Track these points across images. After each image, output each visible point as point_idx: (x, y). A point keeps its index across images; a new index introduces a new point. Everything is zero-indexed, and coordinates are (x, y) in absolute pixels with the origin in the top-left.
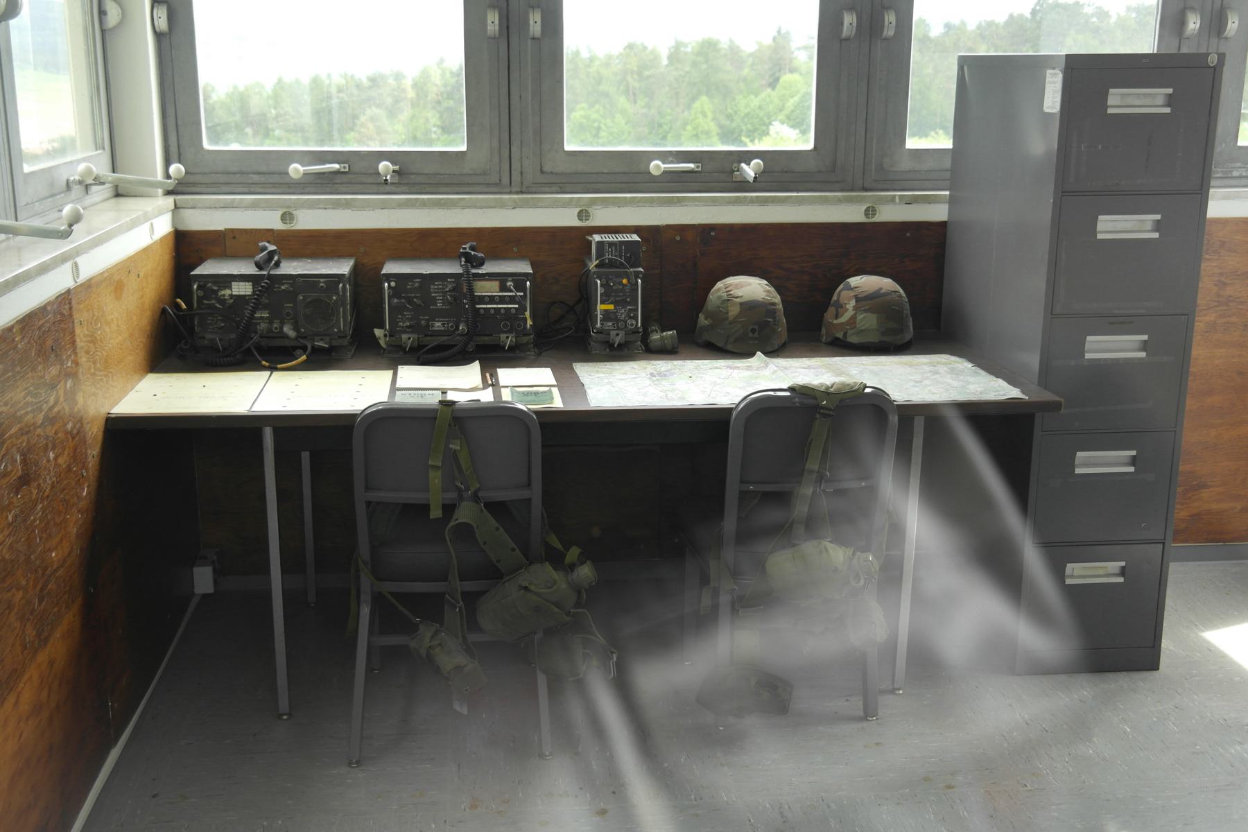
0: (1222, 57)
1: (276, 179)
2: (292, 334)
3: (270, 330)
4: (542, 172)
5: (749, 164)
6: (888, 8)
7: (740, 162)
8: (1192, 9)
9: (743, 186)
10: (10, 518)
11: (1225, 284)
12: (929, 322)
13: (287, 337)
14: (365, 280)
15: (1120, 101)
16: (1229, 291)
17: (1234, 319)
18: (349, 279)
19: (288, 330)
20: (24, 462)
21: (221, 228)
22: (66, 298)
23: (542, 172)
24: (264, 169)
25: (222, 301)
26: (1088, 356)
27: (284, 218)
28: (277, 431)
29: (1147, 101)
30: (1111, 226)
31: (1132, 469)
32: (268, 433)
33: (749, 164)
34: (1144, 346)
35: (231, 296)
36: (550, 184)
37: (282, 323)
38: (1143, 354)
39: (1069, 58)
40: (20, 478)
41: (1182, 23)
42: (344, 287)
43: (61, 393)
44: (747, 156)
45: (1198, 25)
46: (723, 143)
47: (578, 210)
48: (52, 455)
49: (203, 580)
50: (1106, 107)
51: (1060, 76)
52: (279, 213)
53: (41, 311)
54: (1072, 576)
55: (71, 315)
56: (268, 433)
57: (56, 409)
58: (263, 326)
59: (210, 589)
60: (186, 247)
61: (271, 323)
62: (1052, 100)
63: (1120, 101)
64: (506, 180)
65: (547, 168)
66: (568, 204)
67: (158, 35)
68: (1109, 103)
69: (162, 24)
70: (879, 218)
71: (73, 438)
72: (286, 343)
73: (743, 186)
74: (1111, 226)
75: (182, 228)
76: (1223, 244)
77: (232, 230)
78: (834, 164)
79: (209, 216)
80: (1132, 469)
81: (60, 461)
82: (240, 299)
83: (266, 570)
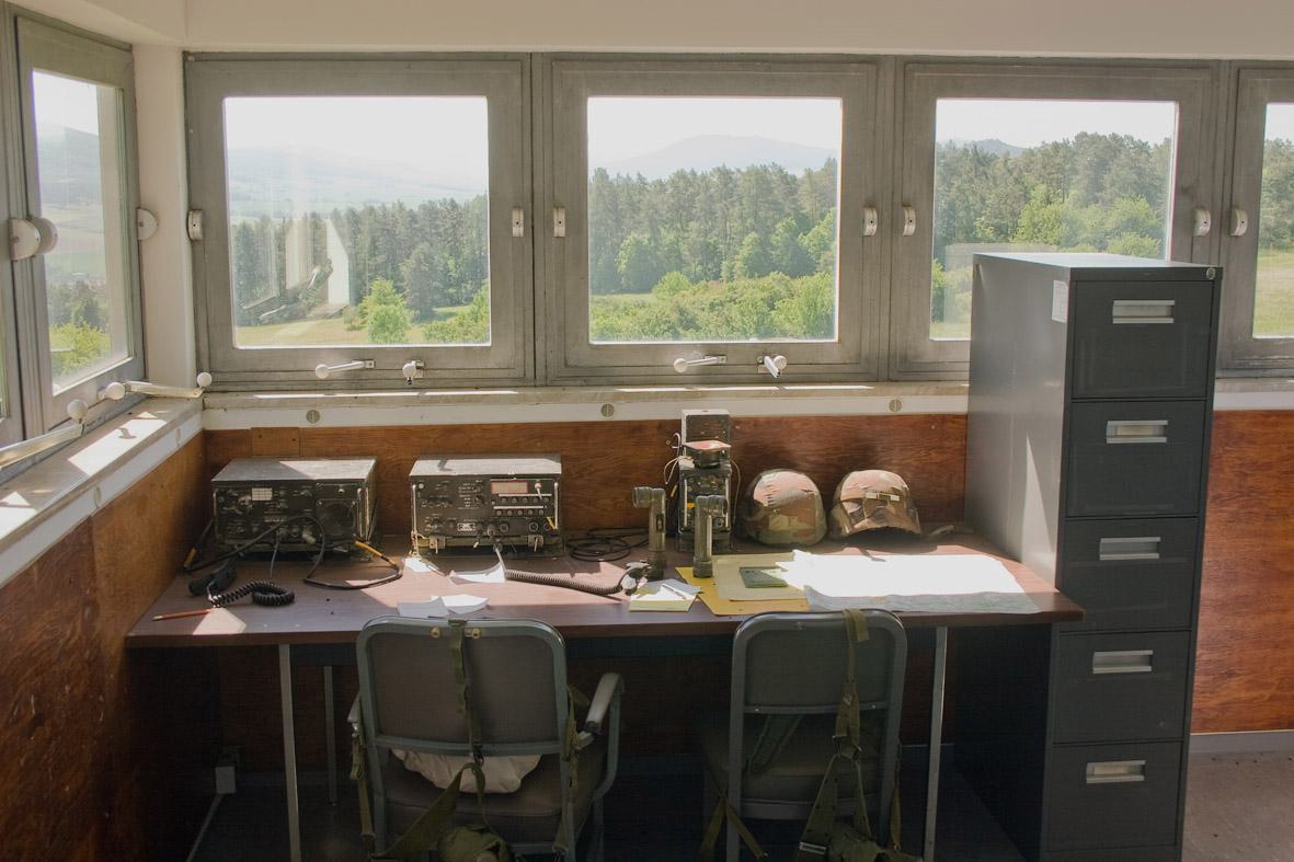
0: (1219, 271)
1: (303, 376)
2: (312, 540)
3: (289, 536)
4: (566, 365)
5: (773, 358)
6: (906, 205)
7: (765, 354)
8: (1203, 208)
9: (767, 379)
10: (22, 762)
11: (1246, 475)
12: (953, 511)
13: (305, 542)
14: (390, 483)
15: (1125, 312)
16: (1250, 481)
17: (1255, 509)
18: (368, 484)
19: (307, 535)
20: (38, 703)
21: (247, 427)
22: (87, 527)
23: (566, 365)
24: (291, 367)
25: (243, 508)
26: (1103, 557)
27: (309, 416)
28: (293, 648)
29: (1155, 312)
30: (1120, 432)
31: (1149, 669)
32: (285, 654)
33: (773, 358)
34: (1158, 547)
35: (251, 501)
36: (576, 377)
37: (302, 529)
38: (1156, 556)
39: (1072, 269)
40: (35, 718)
41: (1193, 222)
42: (363, 492)
43: (79, 623)
44: (769, 351)
45: (1208, 229)
46: (834, 205)
47: (601, 406)
48: (67, 688)
49: (225, 780)
50: (1112, 318)
51: (1067, 288)
52: (304, 413)
53: (62, 545)
54: (1093, 775)
55: (91, 543)
56: (285, 654)
57: (72, 642)
58: (283, 531)
59: (232, 789)
60: (212, 448)
61: (290, 527)
62: (1060, 311)
63: (1125, 312)
64: (530, 374)
65: (571, 362)
66: (592, 399)
67: (193, 242)
68: (1115, 314)
69: (196, 230)
70: (905, 410)
71: (90, 665)
72: (302, 548)
73: (767, 379)
74: (1120, 432)
75: (208, 428)
76: (1242, 436)
77: (258, 429)
78: (859, 355)
79: (233, 417)
80: (1149, 669)
81: (75, 692)
82: (260, 504)
83: (282, 769)
